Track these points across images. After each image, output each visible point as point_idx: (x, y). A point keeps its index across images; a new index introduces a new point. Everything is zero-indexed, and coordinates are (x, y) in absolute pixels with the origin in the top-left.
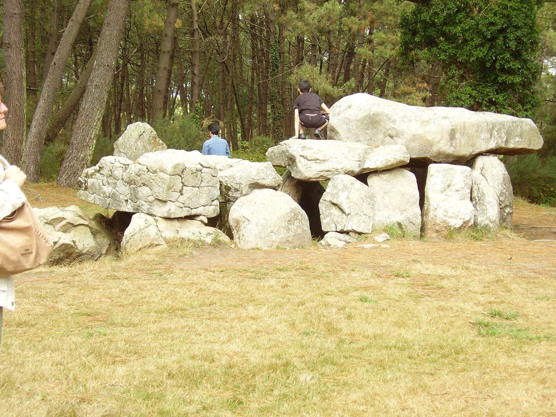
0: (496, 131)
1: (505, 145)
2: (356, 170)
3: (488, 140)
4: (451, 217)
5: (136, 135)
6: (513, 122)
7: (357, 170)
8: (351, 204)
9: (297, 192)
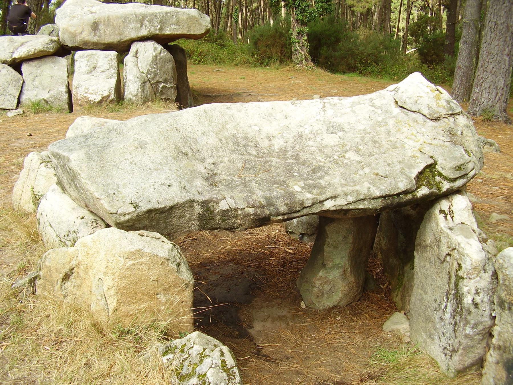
0: (148, 21)
1: (159, 32)
2: (8, 60)
3: (138, 29)
4: (92, 94)
6: (166, 13)
7: (9, 59)
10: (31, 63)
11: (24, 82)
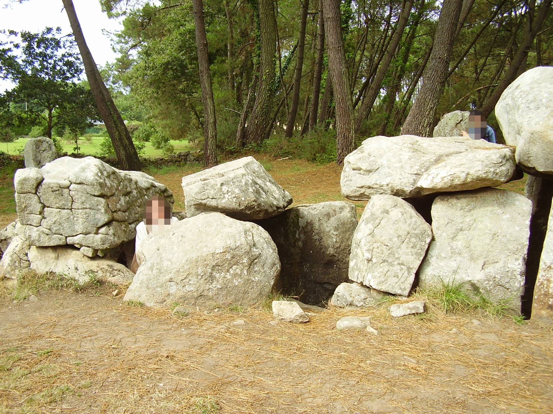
5: (452, 123)
7: (408, 189)
8: (375, 245)
9: (539, 193)
10: (454, 201)
11: (433, 239)
